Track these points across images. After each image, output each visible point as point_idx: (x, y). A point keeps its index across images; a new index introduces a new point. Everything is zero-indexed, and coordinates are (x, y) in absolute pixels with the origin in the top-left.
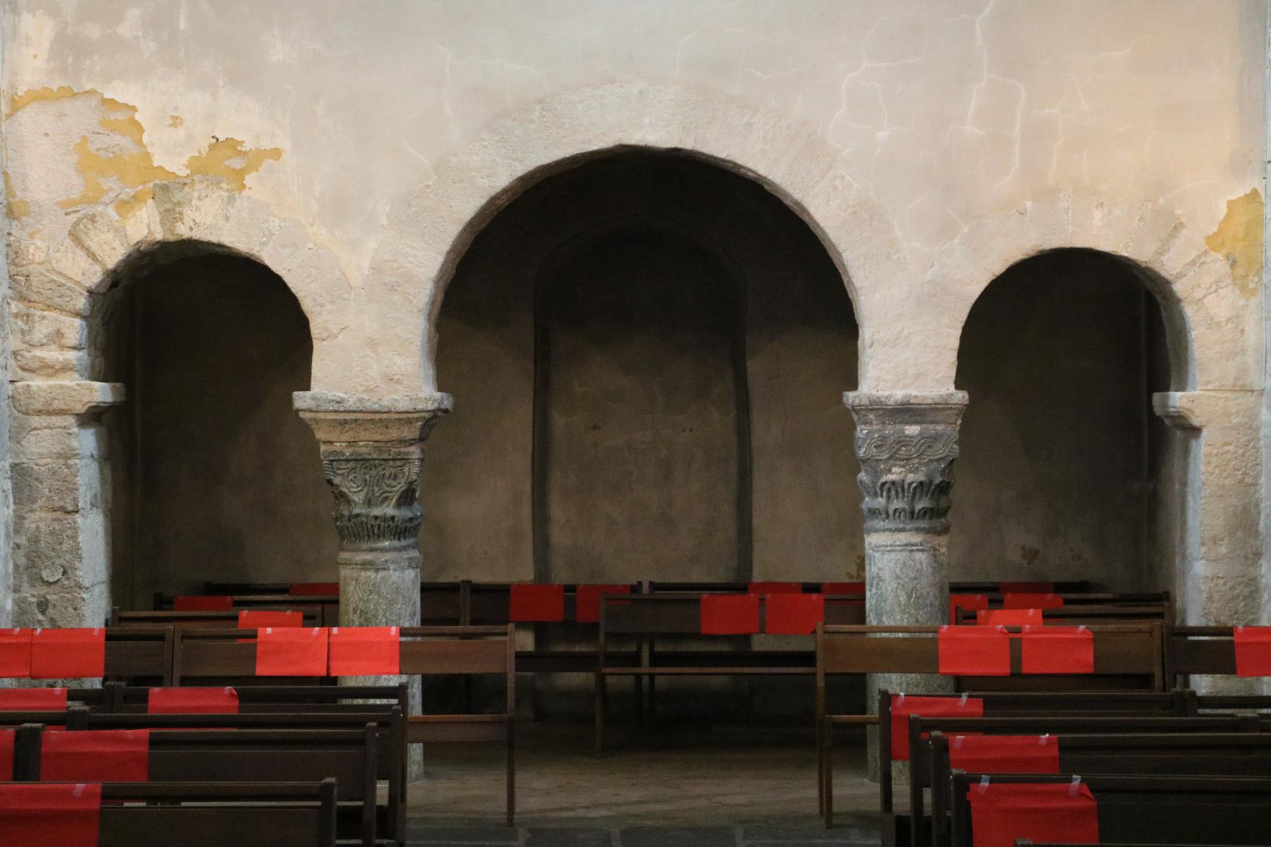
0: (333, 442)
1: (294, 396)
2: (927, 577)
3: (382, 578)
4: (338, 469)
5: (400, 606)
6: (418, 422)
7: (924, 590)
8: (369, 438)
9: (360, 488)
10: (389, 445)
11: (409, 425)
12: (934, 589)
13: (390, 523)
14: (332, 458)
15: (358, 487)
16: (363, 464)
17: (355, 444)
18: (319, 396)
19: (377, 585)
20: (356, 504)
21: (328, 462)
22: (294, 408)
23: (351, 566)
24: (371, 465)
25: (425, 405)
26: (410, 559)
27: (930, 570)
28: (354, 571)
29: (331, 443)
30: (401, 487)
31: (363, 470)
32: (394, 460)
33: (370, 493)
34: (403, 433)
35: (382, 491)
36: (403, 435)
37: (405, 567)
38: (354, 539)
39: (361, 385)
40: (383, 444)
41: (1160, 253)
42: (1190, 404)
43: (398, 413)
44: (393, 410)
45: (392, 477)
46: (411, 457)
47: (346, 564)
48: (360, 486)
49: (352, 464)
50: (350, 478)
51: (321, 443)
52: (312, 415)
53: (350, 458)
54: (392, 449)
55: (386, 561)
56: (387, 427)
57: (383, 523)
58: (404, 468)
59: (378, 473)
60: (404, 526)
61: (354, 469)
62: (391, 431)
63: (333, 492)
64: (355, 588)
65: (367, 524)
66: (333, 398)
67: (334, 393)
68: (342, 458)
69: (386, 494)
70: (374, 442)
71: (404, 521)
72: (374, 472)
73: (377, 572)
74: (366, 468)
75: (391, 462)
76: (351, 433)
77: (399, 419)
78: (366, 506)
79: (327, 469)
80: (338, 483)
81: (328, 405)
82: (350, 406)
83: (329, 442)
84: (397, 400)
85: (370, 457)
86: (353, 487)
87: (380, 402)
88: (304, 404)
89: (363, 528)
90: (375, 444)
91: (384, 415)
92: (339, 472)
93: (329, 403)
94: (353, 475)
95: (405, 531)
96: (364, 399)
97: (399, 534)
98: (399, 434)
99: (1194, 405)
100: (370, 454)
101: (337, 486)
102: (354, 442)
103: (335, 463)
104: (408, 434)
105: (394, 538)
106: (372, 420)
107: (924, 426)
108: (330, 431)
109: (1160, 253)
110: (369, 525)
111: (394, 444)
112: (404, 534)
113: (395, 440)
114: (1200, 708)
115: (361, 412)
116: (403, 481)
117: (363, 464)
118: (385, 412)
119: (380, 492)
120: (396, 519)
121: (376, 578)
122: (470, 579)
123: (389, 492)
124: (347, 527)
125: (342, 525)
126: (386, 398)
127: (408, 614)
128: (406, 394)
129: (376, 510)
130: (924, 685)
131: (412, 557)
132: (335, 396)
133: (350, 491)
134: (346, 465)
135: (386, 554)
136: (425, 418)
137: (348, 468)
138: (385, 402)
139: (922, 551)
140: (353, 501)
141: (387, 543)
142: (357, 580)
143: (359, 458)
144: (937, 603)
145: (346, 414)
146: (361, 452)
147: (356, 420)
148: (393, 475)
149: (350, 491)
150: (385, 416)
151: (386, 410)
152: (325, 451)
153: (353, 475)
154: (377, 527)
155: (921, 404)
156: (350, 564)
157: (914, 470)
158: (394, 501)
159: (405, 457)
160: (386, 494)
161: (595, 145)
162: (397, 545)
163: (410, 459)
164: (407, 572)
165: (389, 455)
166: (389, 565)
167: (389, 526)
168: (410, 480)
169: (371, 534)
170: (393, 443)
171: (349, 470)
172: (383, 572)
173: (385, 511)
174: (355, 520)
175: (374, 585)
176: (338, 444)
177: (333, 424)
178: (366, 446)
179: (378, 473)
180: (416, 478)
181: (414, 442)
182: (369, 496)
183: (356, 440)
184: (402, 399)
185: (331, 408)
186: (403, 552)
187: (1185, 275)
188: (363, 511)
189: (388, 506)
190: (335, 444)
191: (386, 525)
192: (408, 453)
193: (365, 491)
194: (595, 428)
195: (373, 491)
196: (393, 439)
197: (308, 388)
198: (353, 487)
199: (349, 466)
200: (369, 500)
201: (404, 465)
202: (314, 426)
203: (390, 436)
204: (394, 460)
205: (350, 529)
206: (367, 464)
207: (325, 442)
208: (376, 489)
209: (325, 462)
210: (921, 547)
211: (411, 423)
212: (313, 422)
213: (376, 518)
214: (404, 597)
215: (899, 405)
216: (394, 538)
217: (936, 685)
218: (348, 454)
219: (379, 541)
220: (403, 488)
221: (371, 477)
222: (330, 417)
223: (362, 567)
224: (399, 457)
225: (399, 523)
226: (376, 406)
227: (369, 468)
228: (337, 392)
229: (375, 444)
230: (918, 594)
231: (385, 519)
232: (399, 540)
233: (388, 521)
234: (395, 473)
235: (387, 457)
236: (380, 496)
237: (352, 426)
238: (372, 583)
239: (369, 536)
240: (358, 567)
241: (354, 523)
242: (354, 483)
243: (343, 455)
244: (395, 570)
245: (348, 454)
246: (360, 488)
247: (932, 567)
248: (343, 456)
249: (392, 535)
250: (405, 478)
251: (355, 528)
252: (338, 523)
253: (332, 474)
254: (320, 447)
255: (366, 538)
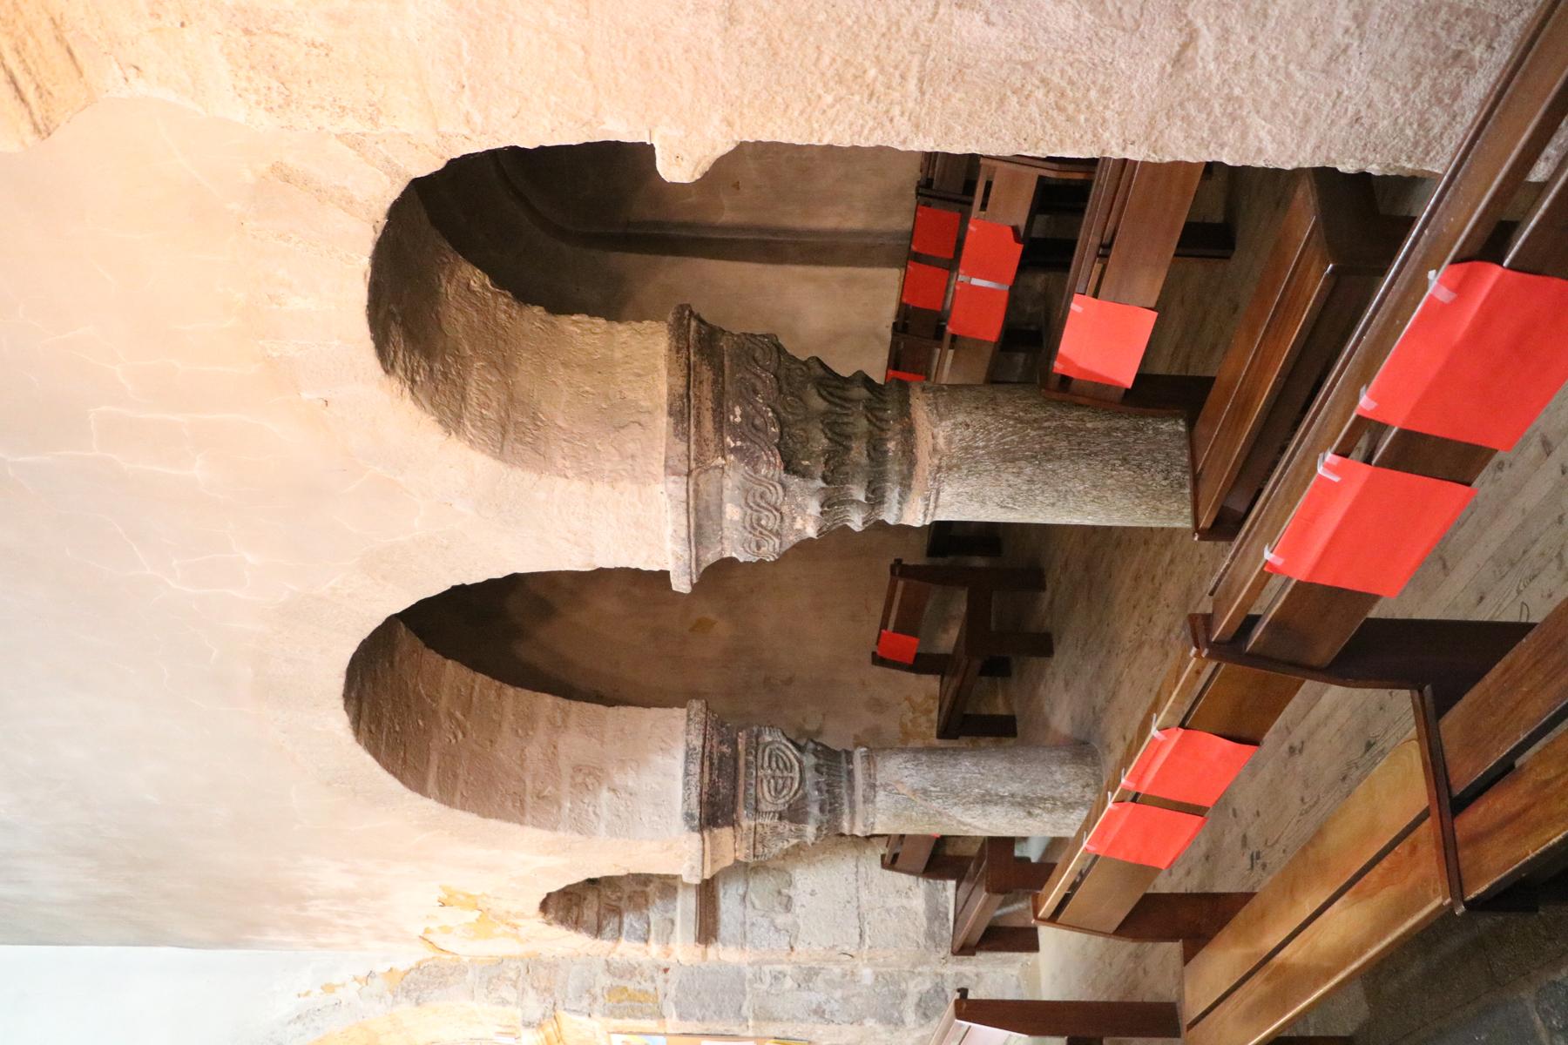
2: (984, 485)
5: (914, 813)
7: (1004, 492)
12: (1005, 476)
27: (972, 480)
41: (348, 203)
42: (684, 164)
99: (686, 157)
107: (725, 500)
109: (348, 203)
114: (1433, 688)
122: (891, 325)
127: (924, 803)
130: (1160, 501)
131: (864, 796)
139: (938, 493)
144: (1028, 470)
155: (689, 526)
157: (802, 508)
187: (388, 161)
194: (737, 186)
210: (932, 499)
214: (905, 809)
215: (690, 547)
217: (1164, 483)
230: (1010, 500)
247: (967, 476)
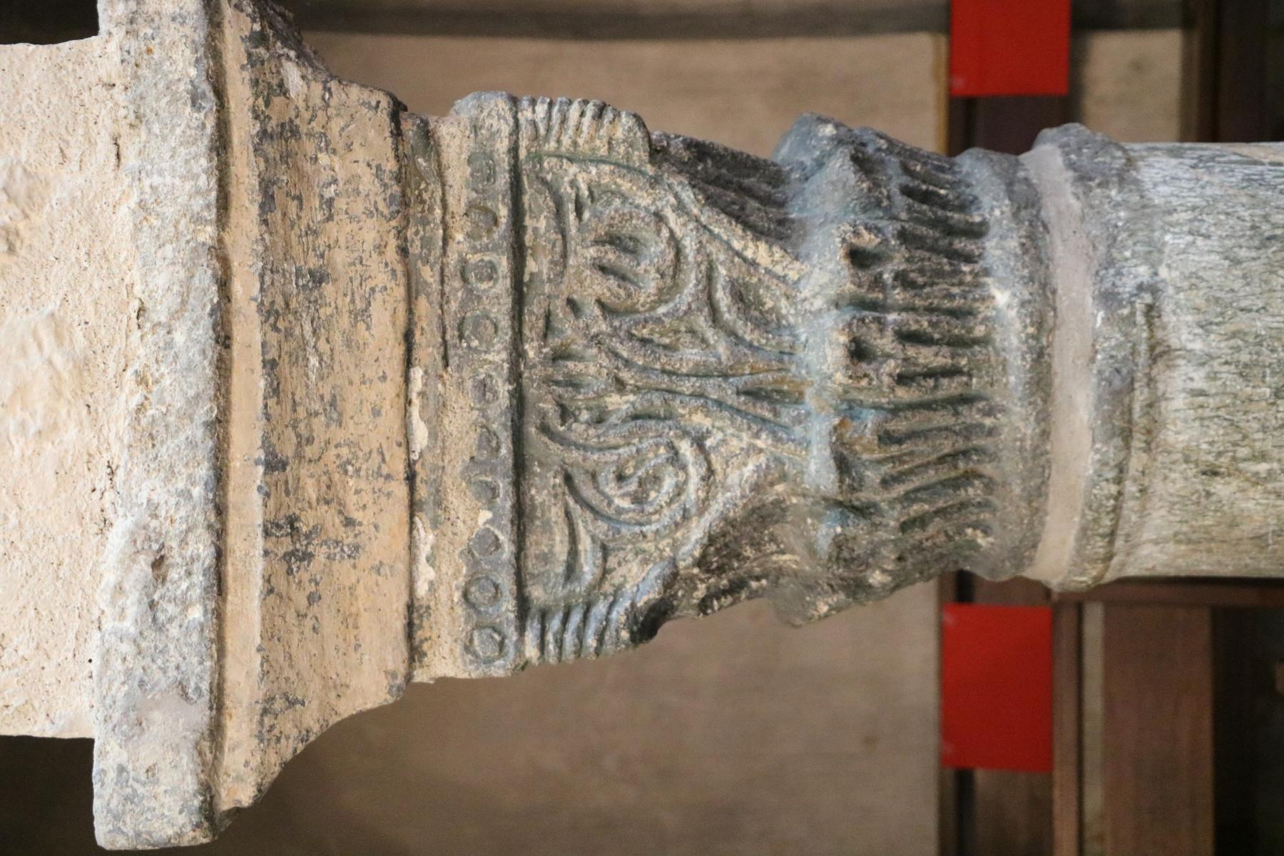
0: (410, 608)
1: (121, 843)
3: (1205, 326)
4: (571, 571)
6: (282, 89)
8: (391, 389)
9: (686, 448)
10: (428, 275)
11: (309, 146)
13: (887, 277)
14: (508, 606)
15: (675, 458)
16: (545, 429)
17: (421, 473)
18: (119, 691)
19: (1244, 357)
20: (777, 472)
21: (531, 636)
22: (194, 836)
23: (1130, 505)
24: (549, 381)
25: (172, 33)
26: (1083, 178)
28: (1158, 486)
29: (413, 614)
30: (680, 208)
31: (578, 430)
32: (519, 253)
33: (713, 388)
34: (353, 179)
35: (701, 321)
36: (368, 183)
37: (1135, 198)
38: (974, 492)
39: (51, 429)
40: (422, 305)
43: (224, 203)
44: (207, 234)
45: (625, 262)
46: (502, 145)
47: (1112, 535)
48: (671, 447)
49: (546, 490)
50: (625, 504)
51: (420, 676)
52: (238, 729)
53: (505, 502)
54: (453, 258)
55: (1108, 298)
56: (319, 278)
57: (892, 317)
58: (566, 190)
59: (596, 340)
60: (901, 201)
61: (568, 479)
62: (340, 258)
63: (704, 606)
64: (1257, 480)
65: (896, 410)
66: (133, 604)
67: (102, 599)
68: (508, 549)
69: (723, 298)
70: (408, 362)
71: (873, 203)
72: (593, 368)
73: (1169, 351)
74: (565, 413)
75: (531, 266)
76: (356, 493)
77: (267, 202)
78: (787, 414)
79: (569, 638)
80: (655, 572)
81: (174, 631)
82: (186, 494)
83: (410, 628)
84: (142, 204)
85: (504, 389)
86: (680, 490)
87: (160, 314)
88: (168, 777)
89: (912, 435)
90: (427, 350)
91: (237, 288)
92: (588, 568)
93: (160, 628)
94: (611, 488)
95: (926, 197)
96: (141, 408)
97: (951, 231)
98: (359, 207)
100: (483, 387)
101: (672, 580)
102: (411, 478)
103: (537, 593)
104: (360, 153)
105: (969, 259)
106: (271, 365)
108: (349, 621)
110: (904, 395)
111: (427, 243)
112: (945, 204)
113: (400, 233)
115: (219, 425)
116: (644, 199)
117: (545, 429)
118: (224, 284)
119: (710, 334)
120: (868, 240)
121: (1205, 360)
123: (710, 277)
124: (904, 527)
125: (889, 554)
126: (135, 275)
128: (104, 149)
129: (810, 356)
132: (119, 589)
133: (703, 506)
134: (547, 527)
135: (1063, 303)
136: (259, 39)
137: (568, 514)
138: (161, 279)
140: (757, 488)
141: (1002, 297)
142: (1213, 473)
143: (505, 451)
145: (233, 522)
146: (473, 437)
147: (274, 464)
148: (611, 256)
149: (703, 506)
150: (245, 288)
151: (204, 278)
152: (468, 648)
153: (611, 488)
154: (911, 351)
156: (1116, 510)
158: (760, 252)
159: (503, 180)
160: (723, 298)
161: (105, 10)
162: (1013, 244)
163: (514, 150)
164: (1160, 195)
165: (490, 272)
166: (1127, 286)
167: (902, 279)
168: (640, 155)
169: (950, 387)
170: (415, 249)
171: (576, 509)
172: (1169, 318)
173: (819, 303)
174: (872, 476)
175: (1244, 373)
176: (425, 574)
177: (300, 599)
178: (437, 411)
179: (596, 340)
180: (626, 121)
181: (409, 127)
182: (731, 399)
183: (399, 468)
184: (138, 175)
185: (196, 613)
186: (1049, 213)
188: (819, 430)
189: (791, 289)
190: (422, 589)
191: (898, 295)
192: (481, 164)
193: (700, 420)
195: (701, 373)
196: (393, 243)
197: (82, 749)
198: (680, 490)
199: (556, 513)
200: (754, 394)
201: (551, 188)
202: (312, 719)
203: (374, 263)
204: (519, 253)
205: (916, 509)
206: (549, 407)
207: (415, 653)
208: (691, 355)
209: (531, 652)
211: (289, 131)
212: (287, 725)
213: (859, 352)
216: (969, 259)
218: (486, 515)
219: (985, 341)
220: (688, 195)
221: (620, 386)
222: (255, 615)
223: (1138, 442)
224: (503, 212)
225: (891, 228)
226: (179, 338)
227: (566, 393)
228: (96, 576)
229: (427, 350)
231: (861, 304)
232: (977, 232)
233: (877, 282)
234: (598, 242)
235: (503, 285)
236: (732, 333)
237: (311, 492)
238: (1238, 386)
239: (966, 400)
240: (1137, 462)
241: (886, 483)
242: (656, 479)
243: (487, 542)
244: (1153, 253)
245: (486, 515)
246: (686, 448)
248: (497, 544)
249: (956, 272)
250: (625, 186)
251: (916, 482)
252: (876, 578)
253: (600, 609)
254: (443, 681)
255: (972, 415)
